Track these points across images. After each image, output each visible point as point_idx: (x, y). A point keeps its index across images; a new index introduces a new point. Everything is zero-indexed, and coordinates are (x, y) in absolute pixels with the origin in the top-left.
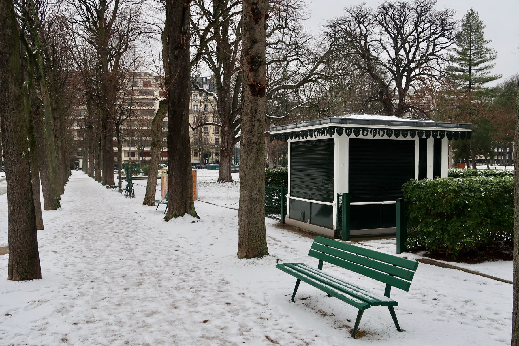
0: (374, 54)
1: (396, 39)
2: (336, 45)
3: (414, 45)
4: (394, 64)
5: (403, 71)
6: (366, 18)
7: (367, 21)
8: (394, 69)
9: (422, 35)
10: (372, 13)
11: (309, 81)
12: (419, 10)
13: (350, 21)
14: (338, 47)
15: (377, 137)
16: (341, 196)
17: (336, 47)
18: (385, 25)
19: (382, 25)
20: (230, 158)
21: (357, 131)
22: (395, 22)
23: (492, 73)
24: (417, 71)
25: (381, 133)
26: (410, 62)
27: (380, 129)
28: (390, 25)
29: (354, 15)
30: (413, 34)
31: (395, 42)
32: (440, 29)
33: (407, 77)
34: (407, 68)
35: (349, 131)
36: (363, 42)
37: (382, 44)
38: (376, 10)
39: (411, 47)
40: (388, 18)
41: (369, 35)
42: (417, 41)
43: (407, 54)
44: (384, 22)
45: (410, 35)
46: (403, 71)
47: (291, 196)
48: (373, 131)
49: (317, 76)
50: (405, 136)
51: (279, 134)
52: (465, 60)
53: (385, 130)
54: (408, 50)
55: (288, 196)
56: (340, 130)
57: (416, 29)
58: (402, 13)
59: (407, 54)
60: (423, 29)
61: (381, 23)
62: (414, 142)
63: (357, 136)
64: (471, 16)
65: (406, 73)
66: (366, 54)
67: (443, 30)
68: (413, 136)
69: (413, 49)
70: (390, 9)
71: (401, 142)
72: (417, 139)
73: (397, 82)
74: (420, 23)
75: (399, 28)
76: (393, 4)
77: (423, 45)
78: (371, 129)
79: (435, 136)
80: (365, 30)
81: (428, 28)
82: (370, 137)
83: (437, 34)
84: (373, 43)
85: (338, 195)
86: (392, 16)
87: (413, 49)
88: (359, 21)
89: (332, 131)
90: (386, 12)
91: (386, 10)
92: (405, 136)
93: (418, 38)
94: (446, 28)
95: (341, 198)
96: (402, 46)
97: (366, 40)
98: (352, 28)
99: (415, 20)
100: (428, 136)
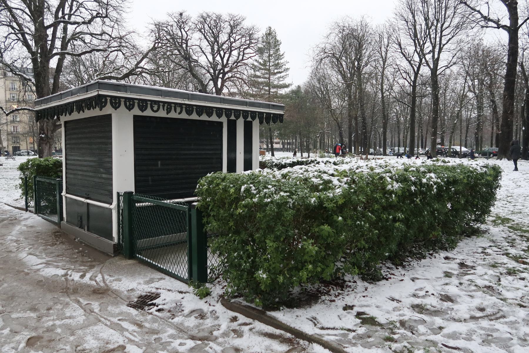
0: (195, 57)
1: (213, 46)
2: (160, 42)
3: (227, 52)
4: (211, 67)
5: (219, 74)
6: (186, 24)
7: (187, 26)
8: (212, 71)
9: (234, 45)
10: (192, 20)
11: (134, 74)
12: (232, 23)
13: (172, 26)
14: (162, 45)
15: (173, 115)
16: (121, 196)
17: (160, 45)
18: (204, 33)
19: (201, 32)
20: (50, 145)
21: (143, 104)
22: (212, 30)
23: (287, 81)
24: (230, 75)
25: (178, 109)
26: (224, 66)
27: (176, 104)
28: (209, 34)
29: (176, 20)
30: (227, 43)
31: (213, 49)
32: (248, 42)
33: (222, 78)
34: (222, 71)
35: (130, 104)
36: (184, 46)
37: (201, 49)
38: (196, 18)
39: (225, 53)
40: (206, 26)
41: (189, 40)
42: (230, 49)
43: (222, 59)
44: (203, 30)
45: (224, 43)
46: (219, 74)
47: (67, 193)
48: (166, 105)
49: (140, 70)
50: (210, 115)
51: (44, 109)
52: (265, 69)
53: (184, 106)
54: (222, 56)
55: (64, 193)
56: (115, 100)
57: (230, 39)
58: (217, 23)
59: (222, 59)
60: (235, 40)
61: (200, 30)
62: (221, 124)
63: (143, 111)
64: (270, 34)
65: (221, 76)
66: (187, 57)
67: (251, 43)
68: (219, 116)
69: (227, 56)
70: (208, 19)
71: (207, 123)
72: (224, 119)
73: (214, 82)
74: (232, 35)
75: (216, 37)
76: (210, 14)
77: (235, 53)
78: (164, 103)
79: (245, 117)
80: (186, 35)
81: (238, 39)
82: (162, 114)
83: (246, 45)
84: (194, 47)
85: (118, 193)
86: (210, 25)
87: (227, 56)
88: (180, 26)
89: (102, 103)
90: (205, 22)
91: (205, 20)
92: (210, 115)
93: (230, 47)
94: (253, 41)
95: (121, 199)
96: (219, 51)
97: (187, 44)
98: (174, 32)
99: (228, 31)
100: (237, 117)
